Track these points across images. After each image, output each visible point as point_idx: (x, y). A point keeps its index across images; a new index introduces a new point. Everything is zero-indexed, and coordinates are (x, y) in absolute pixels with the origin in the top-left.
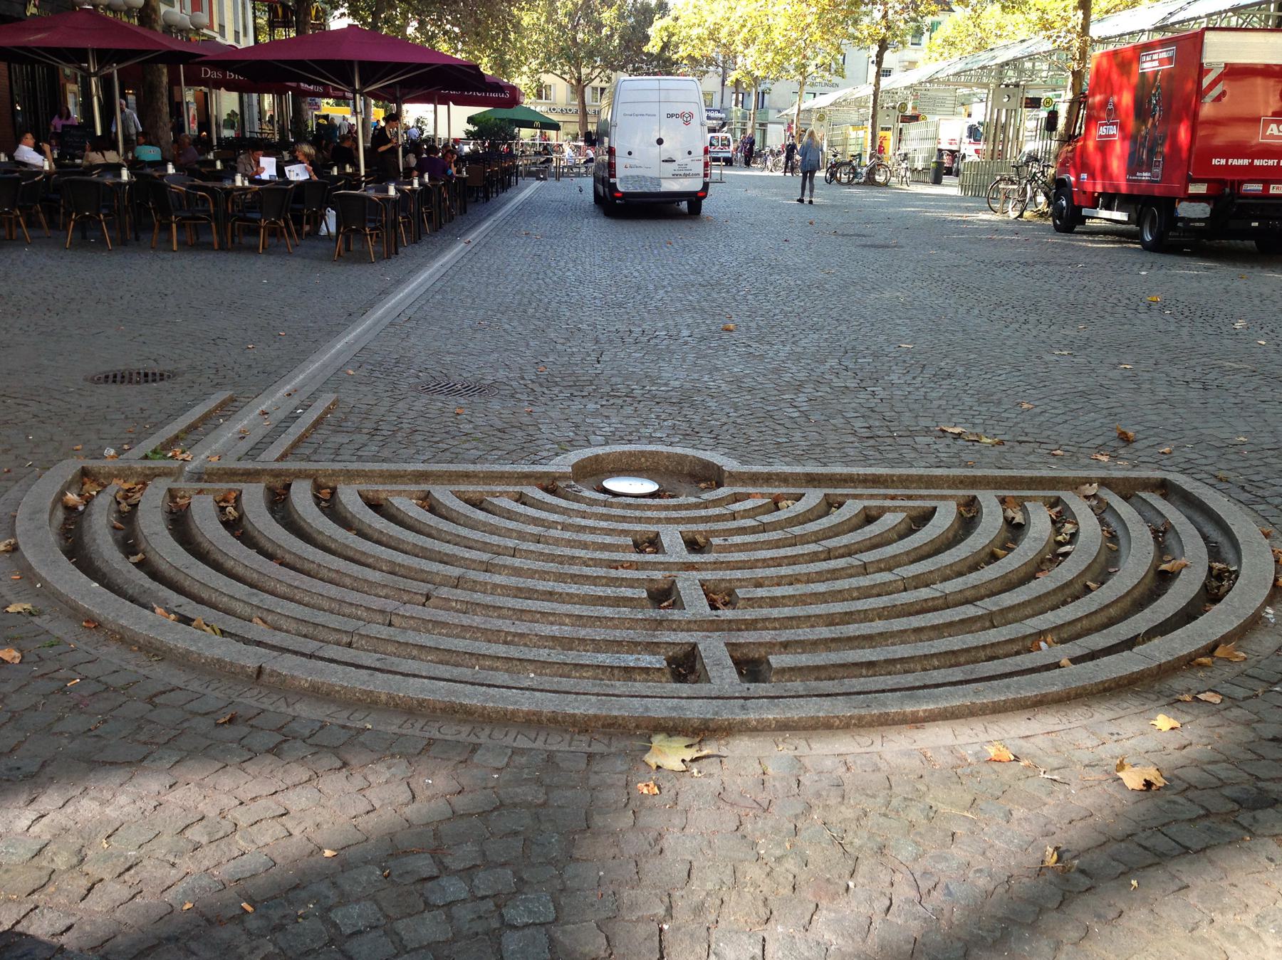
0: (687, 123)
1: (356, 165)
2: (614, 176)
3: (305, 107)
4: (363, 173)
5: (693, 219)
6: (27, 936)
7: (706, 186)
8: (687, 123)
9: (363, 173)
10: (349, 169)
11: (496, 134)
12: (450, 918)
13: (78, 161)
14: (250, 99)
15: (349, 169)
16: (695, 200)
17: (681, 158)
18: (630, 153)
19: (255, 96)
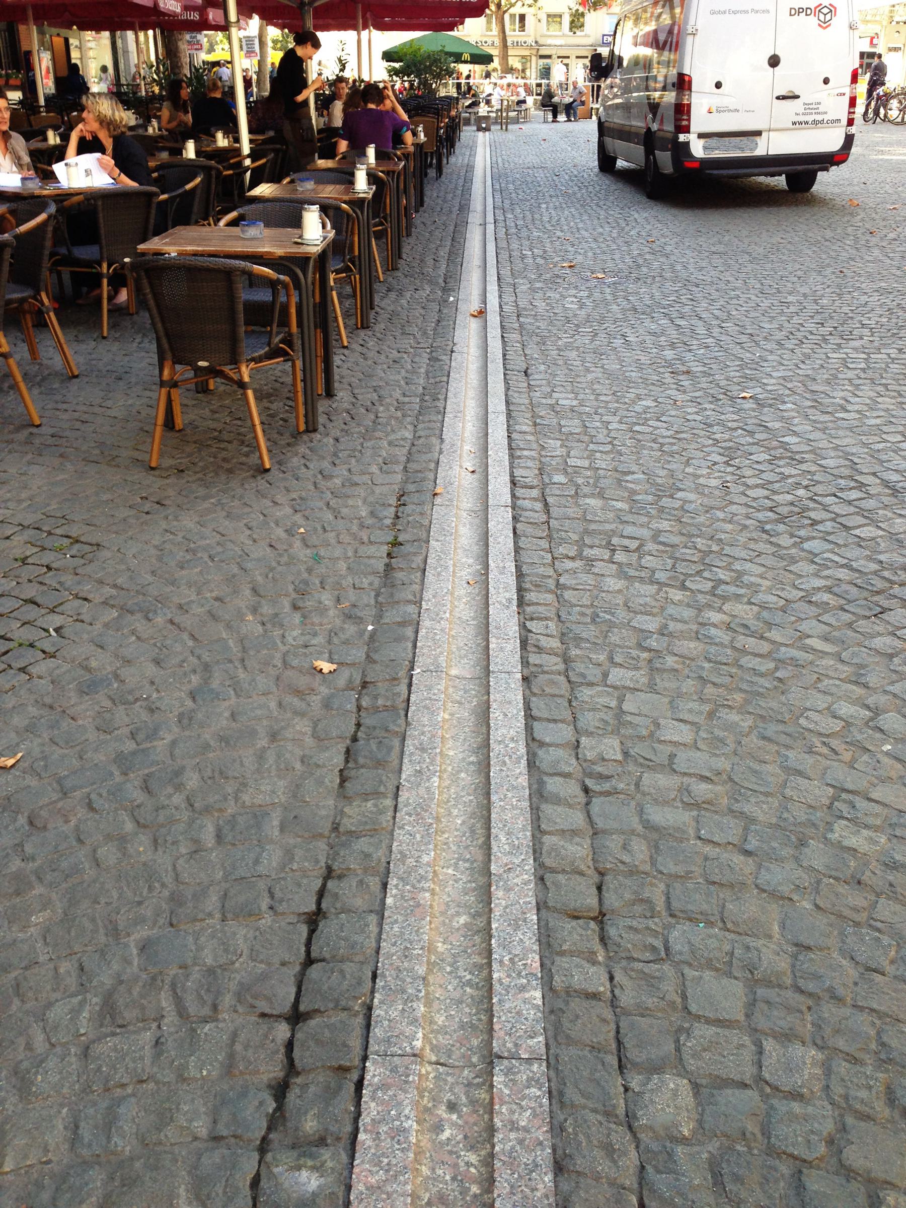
0: (824, 25)
1: (232, 130)
2: (687, 130)
3: (183, 46)
4: (246, 149)
5: (797, 203)
6: (534, 845)
7: (849, 140)
8: (824, 25)
9: (246, 149)
10: (222, 141)
11: (428, 69)
12: (609, 1135)
13: (372, 106)
14: (124, 40)
15: (222, 141)
16: (802, 171)
17: (811, 92)
18: (718, 85)
19: (130, 34)
